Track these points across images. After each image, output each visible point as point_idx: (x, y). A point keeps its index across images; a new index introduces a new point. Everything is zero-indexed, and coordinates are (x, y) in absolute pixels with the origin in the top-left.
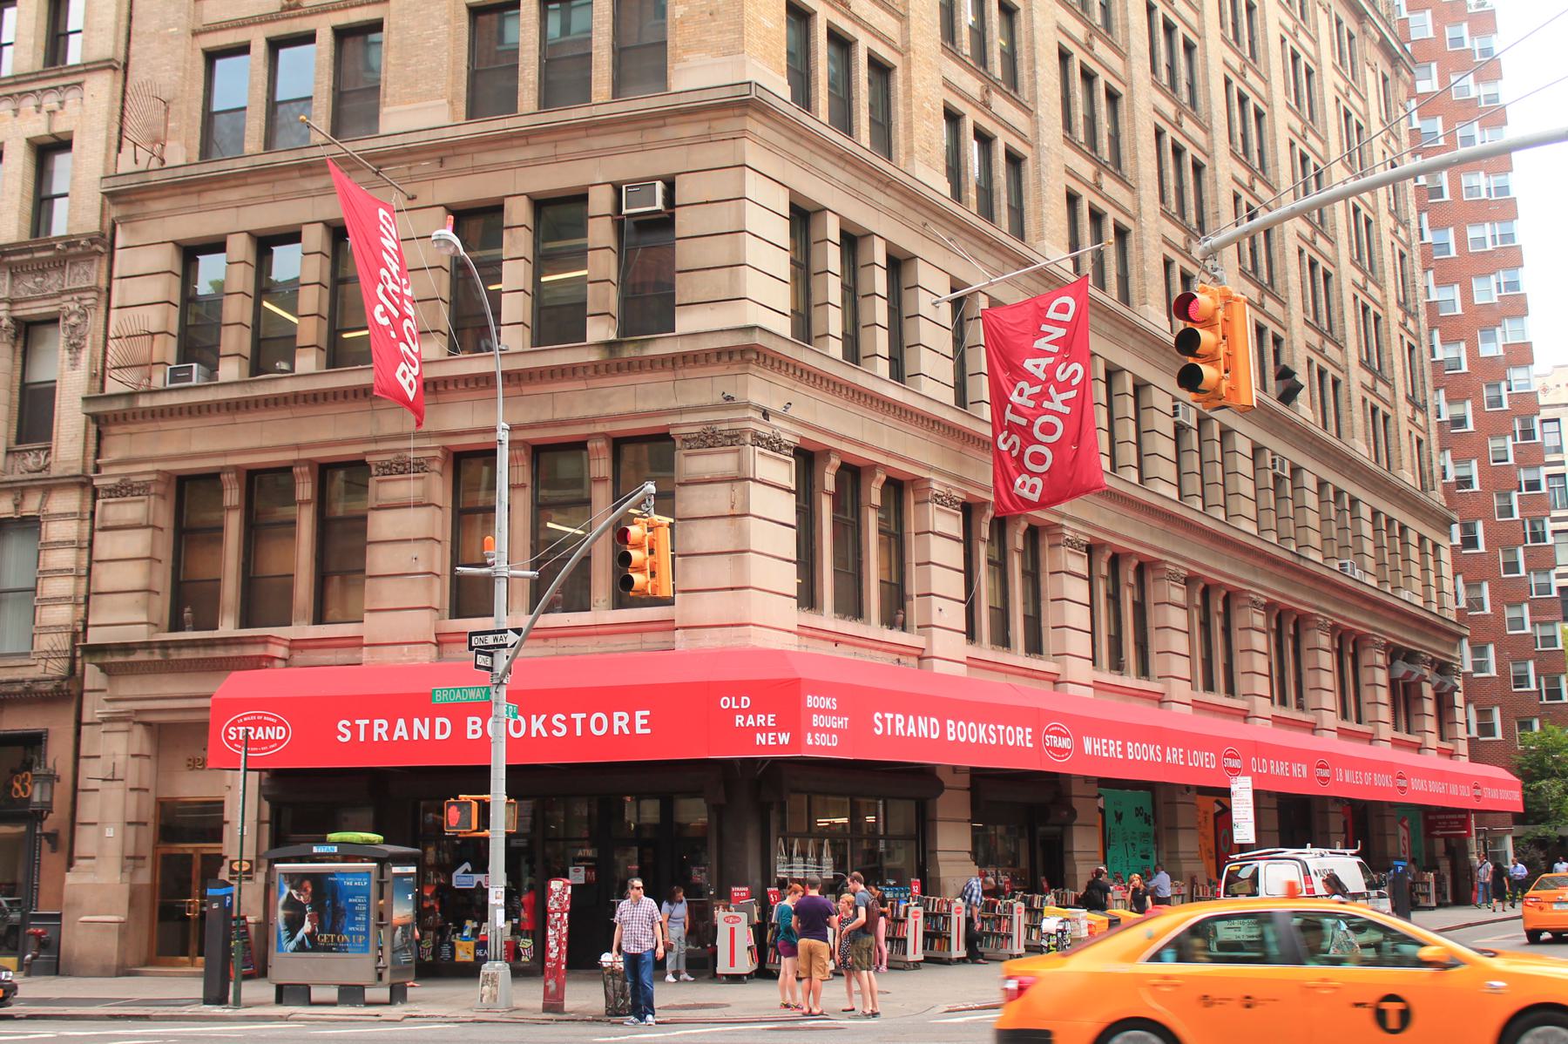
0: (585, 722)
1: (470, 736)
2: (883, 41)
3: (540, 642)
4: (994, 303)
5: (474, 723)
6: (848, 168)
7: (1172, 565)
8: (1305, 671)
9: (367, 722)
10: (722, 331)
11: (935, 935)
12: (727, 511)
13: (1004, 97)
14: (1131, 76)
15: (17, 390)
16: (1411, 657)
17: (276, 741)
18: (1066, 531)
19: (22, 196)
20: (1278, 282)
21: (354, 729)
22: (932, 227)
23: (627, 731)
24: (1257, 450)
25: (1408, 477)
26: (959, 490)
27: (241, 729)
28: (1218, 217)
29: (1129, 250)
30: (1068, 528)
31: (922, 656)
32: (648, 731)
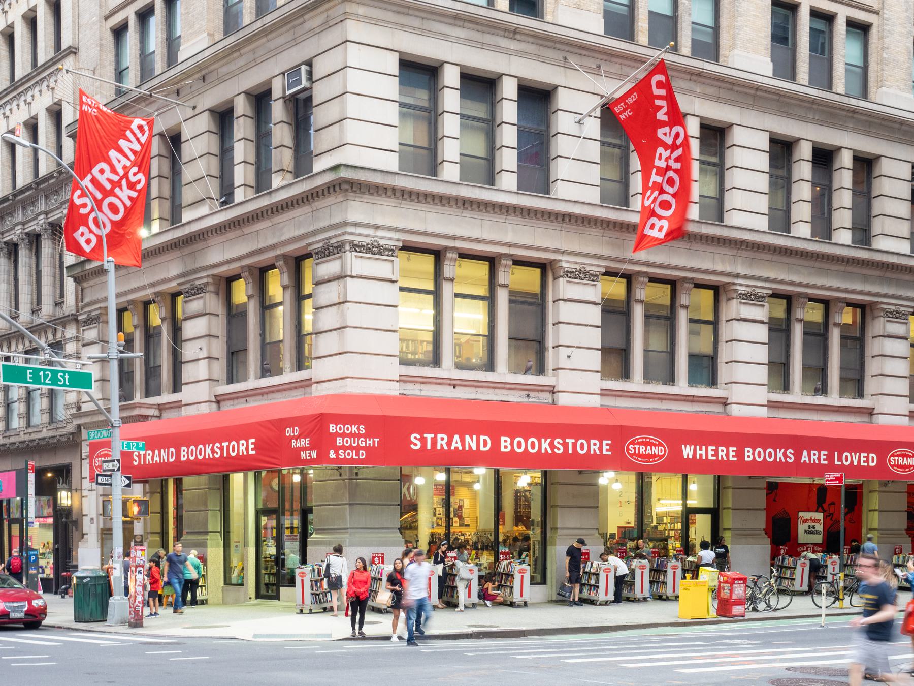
0: (574, 445)
1: (503, 449)
3: (260, 397)
6: (466, 24)
10: (324, 171)
12: (336, 301)
17: (658, 455)
18: (738, 288)
21: (423, 441)
23: (598, 452)
27: (637, 446)
29: (870, 42)
30: (741, 285)
31: (553, 391)
32: (609, 453)
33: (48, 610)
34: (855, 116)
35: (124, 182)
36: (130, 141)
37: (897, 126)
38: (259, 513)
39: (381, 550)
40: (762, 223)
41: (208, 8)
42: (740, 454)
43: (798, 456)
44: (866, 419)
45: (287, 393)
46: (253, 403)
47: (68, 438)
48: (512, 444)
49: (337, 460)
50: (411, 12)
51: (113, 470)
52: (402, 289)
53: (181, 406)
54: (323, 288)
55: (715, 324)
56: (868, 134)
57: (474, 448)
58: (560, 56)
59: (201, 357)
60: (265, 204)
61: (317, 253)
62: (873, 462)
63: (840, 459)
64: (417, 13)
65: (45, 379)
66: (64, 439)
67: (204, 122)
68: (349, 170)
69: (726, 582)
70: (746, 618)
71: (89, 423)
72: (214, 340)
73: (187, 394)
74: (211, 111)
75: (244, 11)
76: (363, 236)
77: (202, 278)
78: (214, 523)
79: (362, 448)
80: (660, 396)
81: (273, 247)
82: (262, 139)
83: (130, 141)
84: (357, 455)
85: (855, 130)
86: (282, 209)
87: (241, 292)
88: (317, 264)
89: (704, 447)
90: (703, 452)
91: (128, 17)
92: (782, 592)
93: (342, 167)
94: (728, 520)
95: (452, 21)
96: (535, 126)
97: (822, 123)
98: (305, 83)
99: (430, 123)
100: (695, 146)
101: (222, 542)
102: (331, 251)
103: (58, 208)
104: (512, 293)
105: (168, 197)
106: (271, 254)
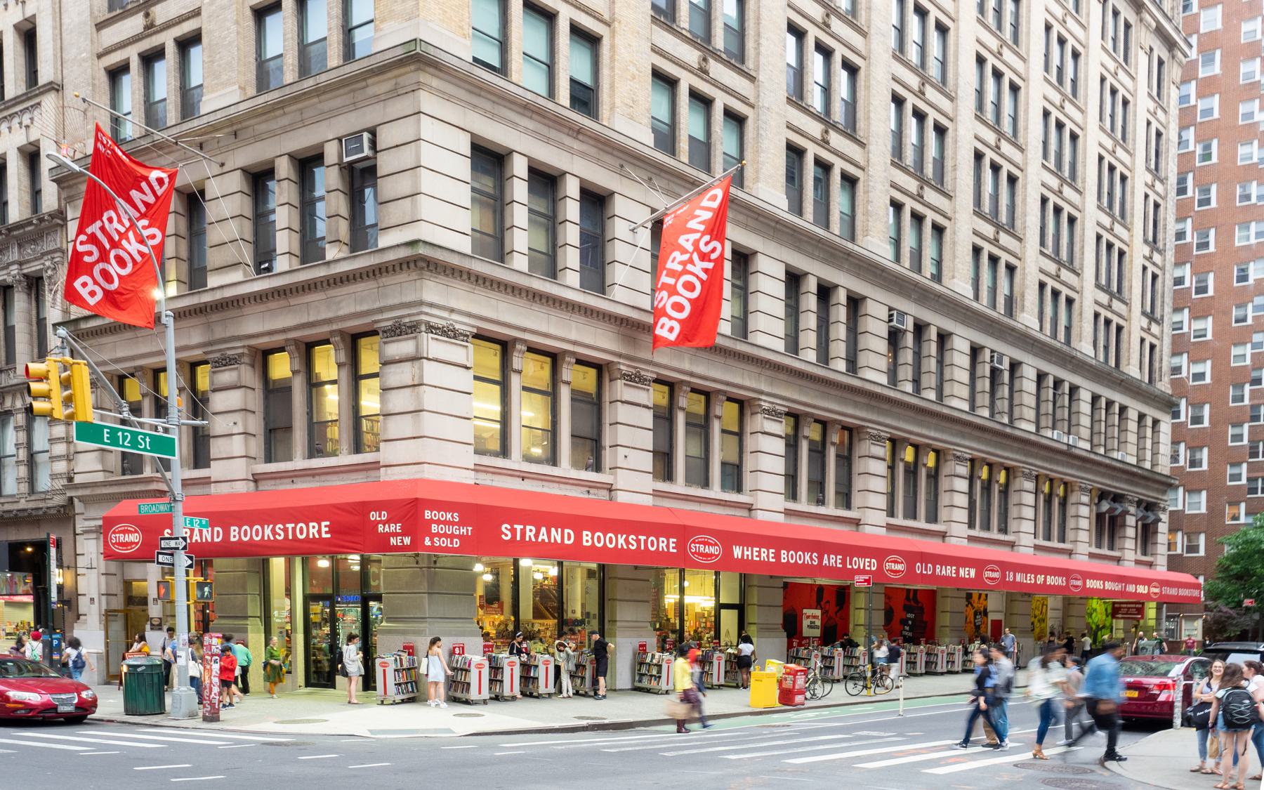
2: (587, 13)
3: (310, 478)
6: (534, 116)
7: (873, 429)
8: (1010, 506)
10: (398, 246)
11: (528, 679)
12: (410, 383)
13: (725, 65)
14: (869, 51)
15: (34, 323)
16: (1117, 498)
18: (763, 403)
19: (19, 189)
20: (1018, 223)
21: (513, 531)
22: (628, 168)
24: (975, 351)
25: (1133, 369)
26: (628, 366)
28: (955, 170)
29: (857, 194)
30: (765, 401)
31: (610, 489)
33: (98, 703)
34: (850, 258)
35: (131, 234)
36: (144, 193)
37: (879, 272)
38: (309, 599)
39: (460, 640)
40: (780, 346)
41: (239, 59)
42: (777, 556)
43: (821, 559)
44: (854, 528)
45: (345, 476)
46: (301, 485)
47: (59, 511)
48: (592, 538)
49: (432, 548)
50: (483, 93)
51: (178, 549)
52: (476, 378)
53: (210, 483)
54: (392, 369)
55: (740, 435)
56: (858, 276)
58: (617, 163)
59: (235, 431)
60: (322, 274)
61: (384, 332)
62: (218, 537)
63: (851, 564)
64: (489, 96)
65: (123, 442)
66: (53, 511)
67: (236, 181)
68: (428, 247)
69: (789, 674)
70: (806, 706)
71: (89, 496)
72: (250, 416)
73: (216, 470)
74: (244, 170)
75: (285, 68)
76: (438, 318)
77: (237, 348)
78: (254, 608)
79: (456, 536)
81: (329, 321)
82: (307, 206)
83: (144, 193)
84: (452, 543)
85: (848, 271)
86: (342, 282)
87: (281, 367)
88: (385, 343)
90: (749, 553)
91: (129, 58)
92: (824, 681)
93: (421, 244)
94: (752, 615)
95: (521, 110)
96: (591, 228)
97: (825, 261)
98: (367, 152)
99: (495, 212)
100: (728, 266)
101: (262, 628)
102: (400, 330)
103: (36, 259)
104: (573, 391)
105: (185, 258)
106: (326, 329)
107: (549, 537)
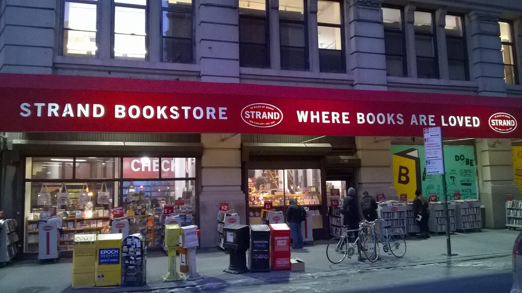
1: (359, 122)
4: (57, 197)
5: (120, 109)
9: (44, 104)
17: (274, 120)
23: (214, 118)
27: (253, 112)
32: (226, 118)
43: (407, 119)
48: (365, 118)
57: (87, 114)
62: (476, 123)
63: (447, 121)
80: (187, 73)
89: (318, 113)
107: (418, 121)
